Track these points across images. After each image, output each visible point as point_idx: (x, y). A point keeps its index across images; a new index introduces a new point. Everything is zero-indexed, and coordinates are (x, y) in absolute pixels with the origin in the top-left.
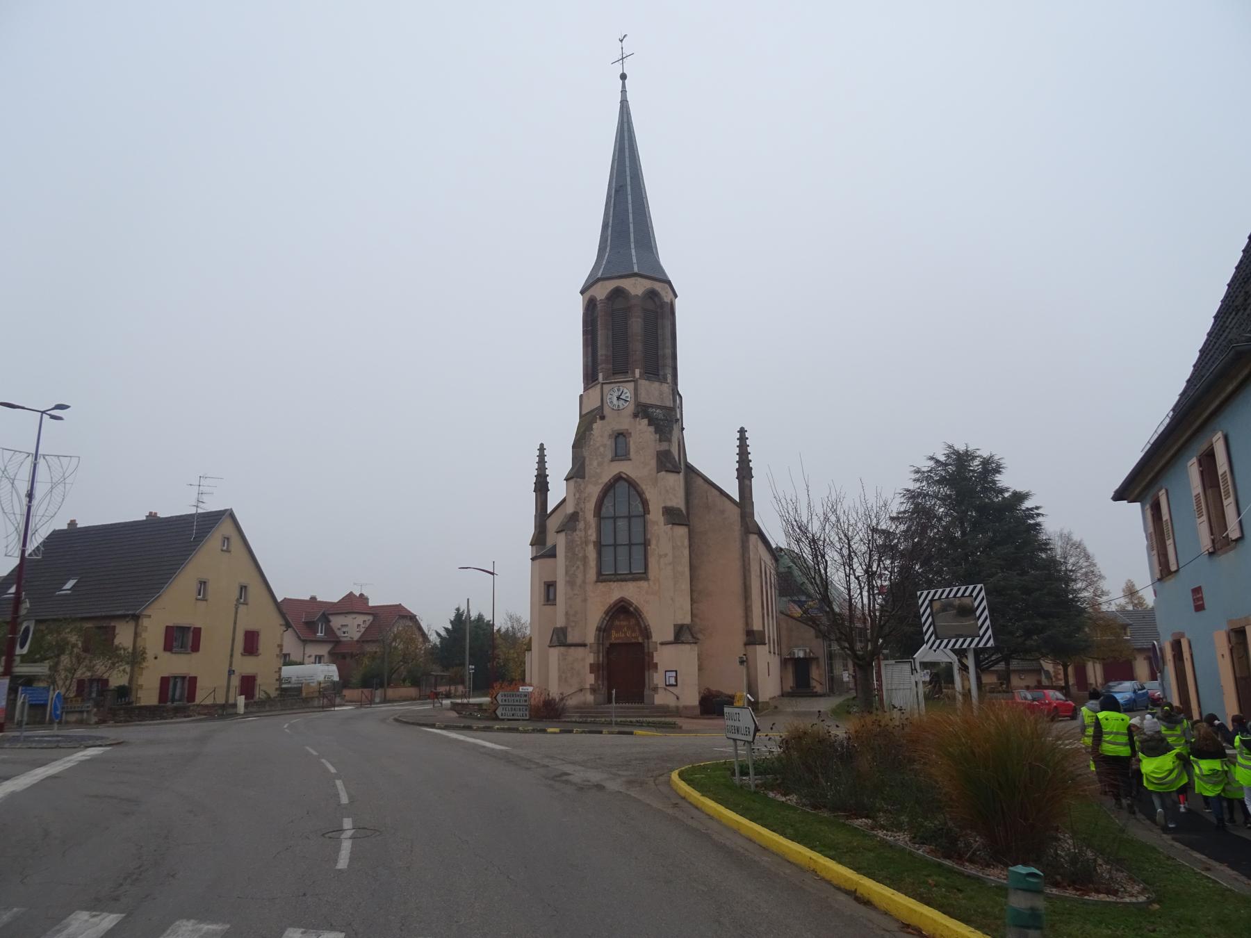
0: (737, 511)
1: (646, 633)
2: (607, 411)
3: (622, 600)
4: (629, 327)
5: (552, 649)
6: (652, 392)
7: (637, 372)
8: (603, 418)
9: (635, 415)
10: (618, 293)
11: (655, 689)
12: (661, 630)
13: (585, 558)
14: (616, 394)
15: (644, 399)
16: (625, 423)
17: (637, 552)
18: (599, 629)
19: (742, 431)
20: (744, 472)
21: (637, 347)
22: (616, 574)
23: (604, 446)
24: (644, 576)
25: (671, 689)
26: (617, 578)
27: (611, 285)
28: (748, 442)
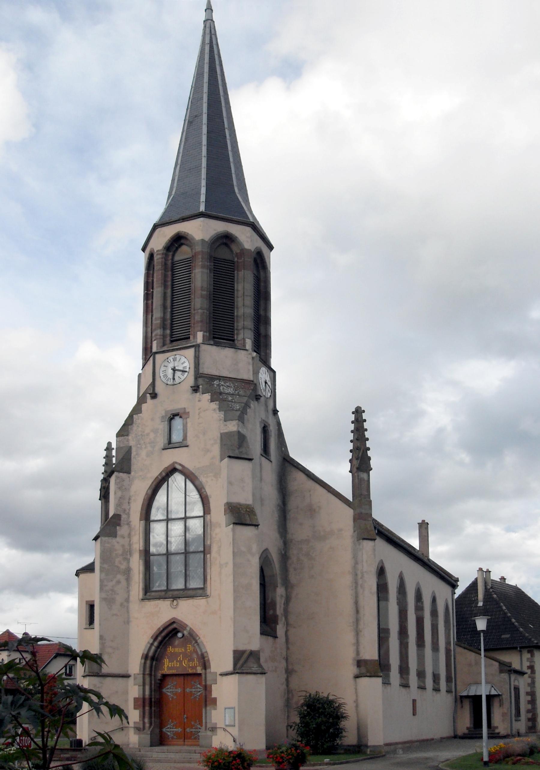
0: (349, 513)
1: (205, 665)
2: (159, 389)
3: (173, 622)
4: (209, 284)
5: (364, 681)
6: (223, 361)
7: (200, 337)
8: (154, 396)
9: (195, 389)
10: (178, 240)
11: (214, 729)
12: (221, 659)
13: (128, 572)
14: (171, 365)
15: (208, 368)
16: (183, 399)
17: (195, 561)
18: (146, 657)
19: (358, 412)
20: (361, 462)
21: (199, 304)
22: (167, 590)
23: (155, 431)
24: (201, 592)
25: (228, 729)
26: (172, 595)
27: (170, 231)
28: (366, 425)
